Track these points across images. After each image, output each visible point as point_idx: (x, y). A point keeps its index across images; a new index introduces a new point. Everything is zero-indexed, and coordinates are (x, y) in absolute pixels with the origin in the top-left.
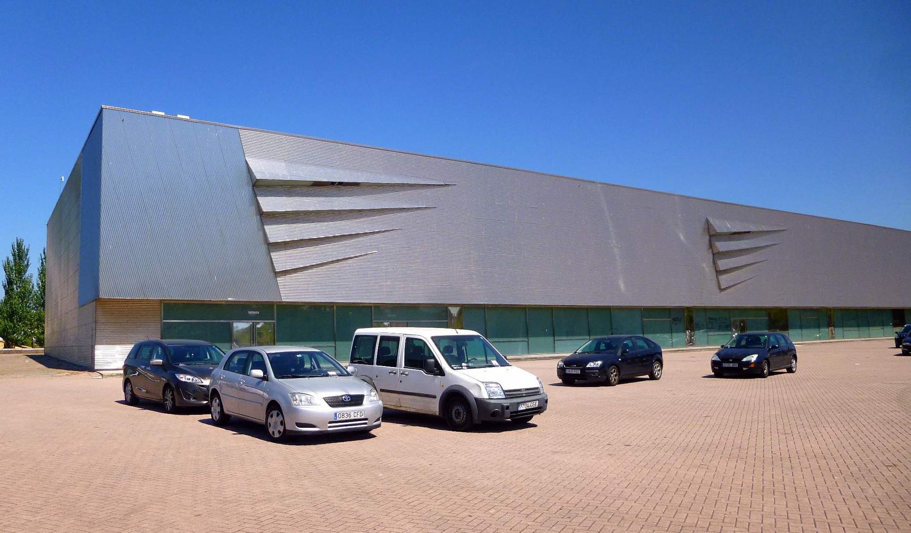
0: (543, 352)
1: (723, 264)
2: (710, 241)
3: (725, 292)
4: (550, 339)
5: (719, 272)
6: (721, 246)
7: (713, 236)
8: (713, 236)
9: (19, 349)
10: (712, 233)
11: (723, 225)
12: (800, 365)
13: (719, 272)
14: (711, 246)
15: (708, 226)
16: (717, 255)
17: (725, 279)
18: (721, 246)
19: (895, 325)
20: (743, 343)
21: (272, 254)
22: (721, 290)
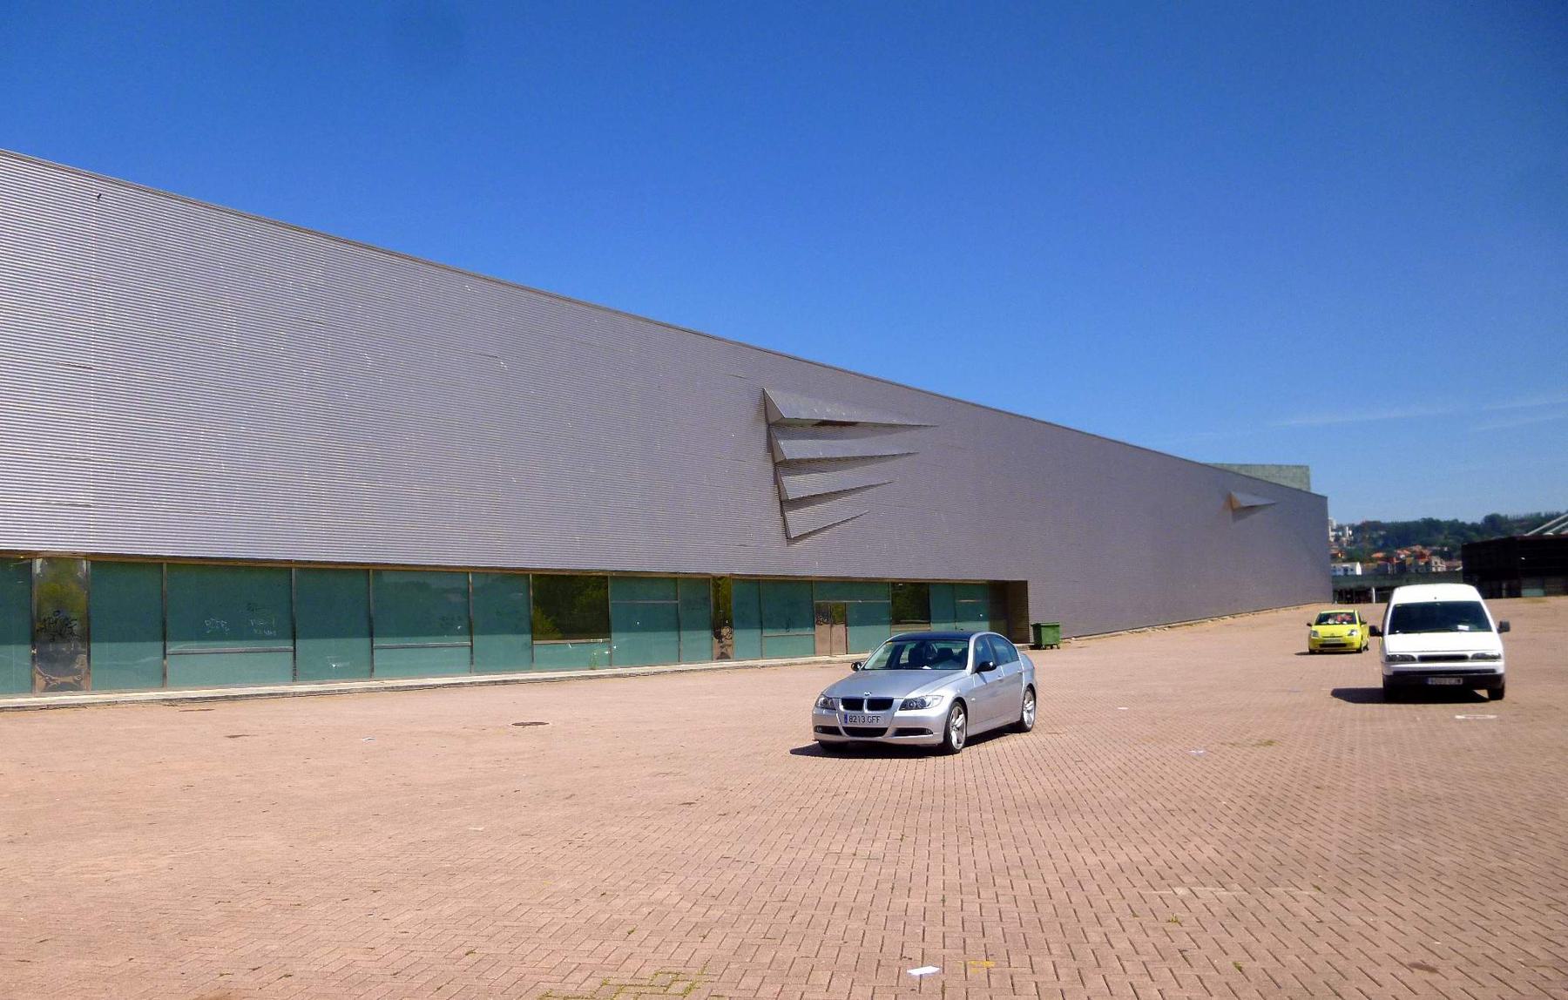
0: (513, 671)
1: (797, 485)
2: (769, 436)
3: (798, 545)
4: (670, 637)
5: (786, 504)
6: (792, 448)
7: (776, 426)
8: (776, 426)
9: (827, 658)
10: (772, 420)
11: (790, 405)
12: (1508, 693)
13: (786, 504)
14: (771, 447)
15: (766, 404)
16: (783, 466)
17: (799, 520)
18: (792, 448)
19: (897, 620)
20: (905, 657)
21: (785, 479)
22: (790, 540)
